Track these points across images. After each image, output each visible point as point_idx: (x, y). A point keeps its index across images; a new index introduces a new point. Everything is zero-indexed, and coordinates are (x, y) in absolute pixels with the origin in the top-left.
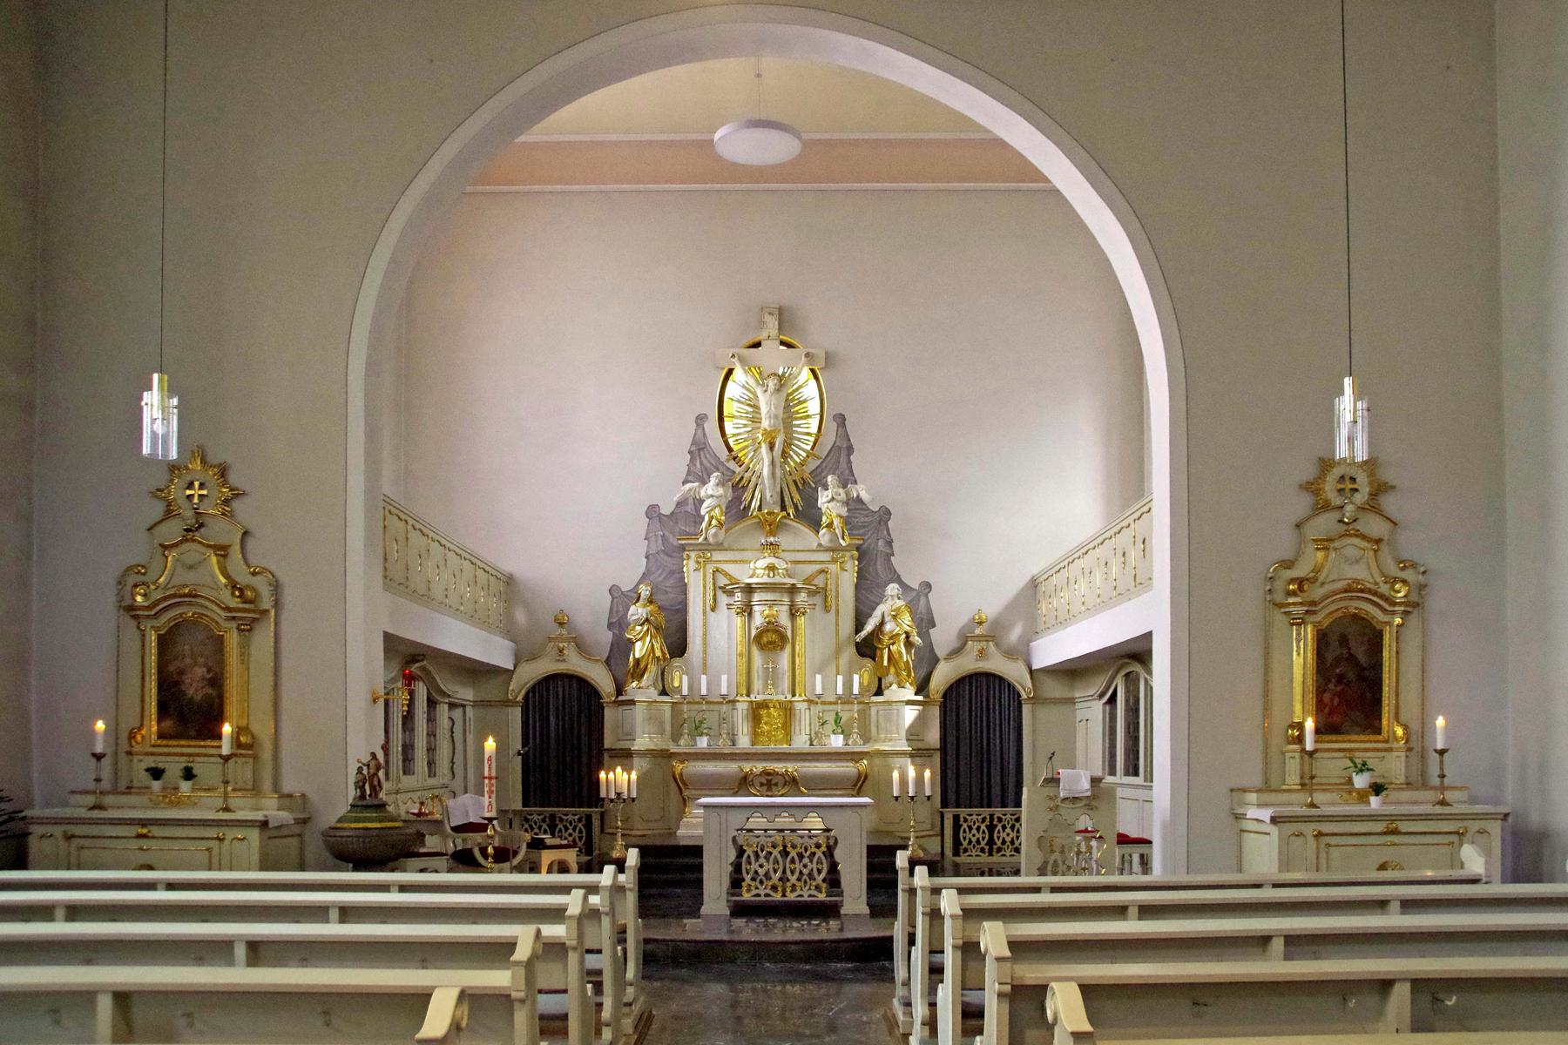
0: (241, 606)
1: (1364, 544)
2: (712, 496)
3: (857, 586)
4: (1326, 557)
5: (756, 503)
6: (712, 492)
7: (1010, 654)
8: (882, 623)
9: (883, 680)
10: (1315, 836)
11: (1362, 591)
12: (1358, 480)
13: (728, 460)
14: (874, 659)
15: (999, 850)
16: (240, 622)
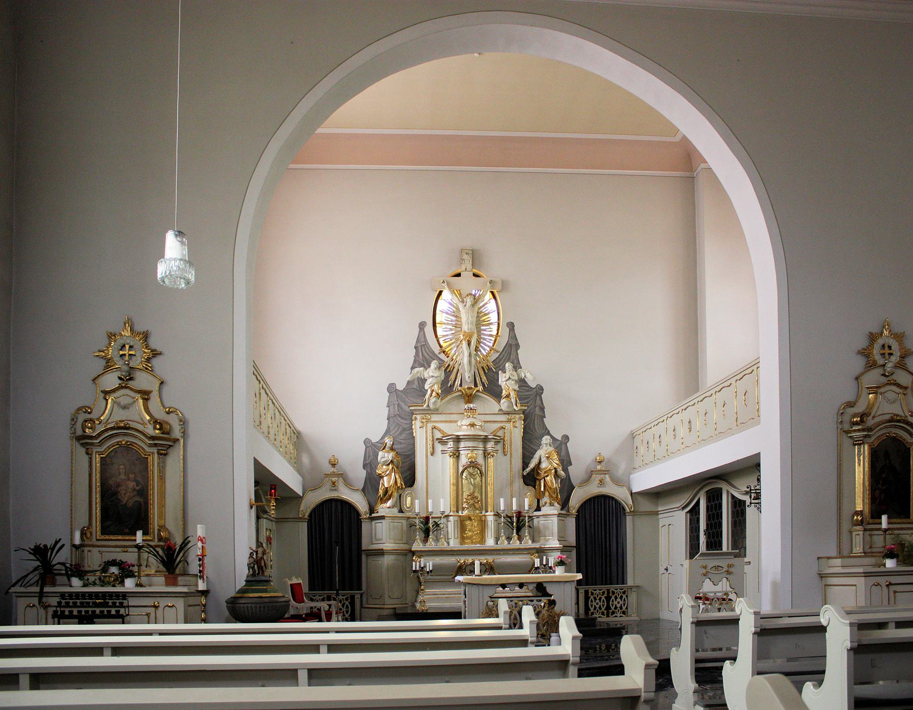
0: (161, 435)
1: (898, 390)
2: (433, 376)
3: (523, 438)
4: (876, 398)
5: (458, 382)
6: (432, 375)
7: (617, 482)
8: (540, 463)
9: (541, 501)
10: (887, 586)
11: (899, 421)
12: (892, 348)
13: (439, 353)
14: (534, 487)
15: (613, 613)
16: (160, 448)
